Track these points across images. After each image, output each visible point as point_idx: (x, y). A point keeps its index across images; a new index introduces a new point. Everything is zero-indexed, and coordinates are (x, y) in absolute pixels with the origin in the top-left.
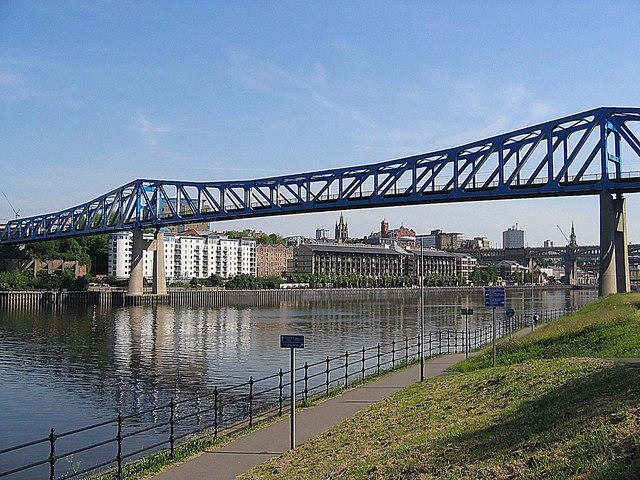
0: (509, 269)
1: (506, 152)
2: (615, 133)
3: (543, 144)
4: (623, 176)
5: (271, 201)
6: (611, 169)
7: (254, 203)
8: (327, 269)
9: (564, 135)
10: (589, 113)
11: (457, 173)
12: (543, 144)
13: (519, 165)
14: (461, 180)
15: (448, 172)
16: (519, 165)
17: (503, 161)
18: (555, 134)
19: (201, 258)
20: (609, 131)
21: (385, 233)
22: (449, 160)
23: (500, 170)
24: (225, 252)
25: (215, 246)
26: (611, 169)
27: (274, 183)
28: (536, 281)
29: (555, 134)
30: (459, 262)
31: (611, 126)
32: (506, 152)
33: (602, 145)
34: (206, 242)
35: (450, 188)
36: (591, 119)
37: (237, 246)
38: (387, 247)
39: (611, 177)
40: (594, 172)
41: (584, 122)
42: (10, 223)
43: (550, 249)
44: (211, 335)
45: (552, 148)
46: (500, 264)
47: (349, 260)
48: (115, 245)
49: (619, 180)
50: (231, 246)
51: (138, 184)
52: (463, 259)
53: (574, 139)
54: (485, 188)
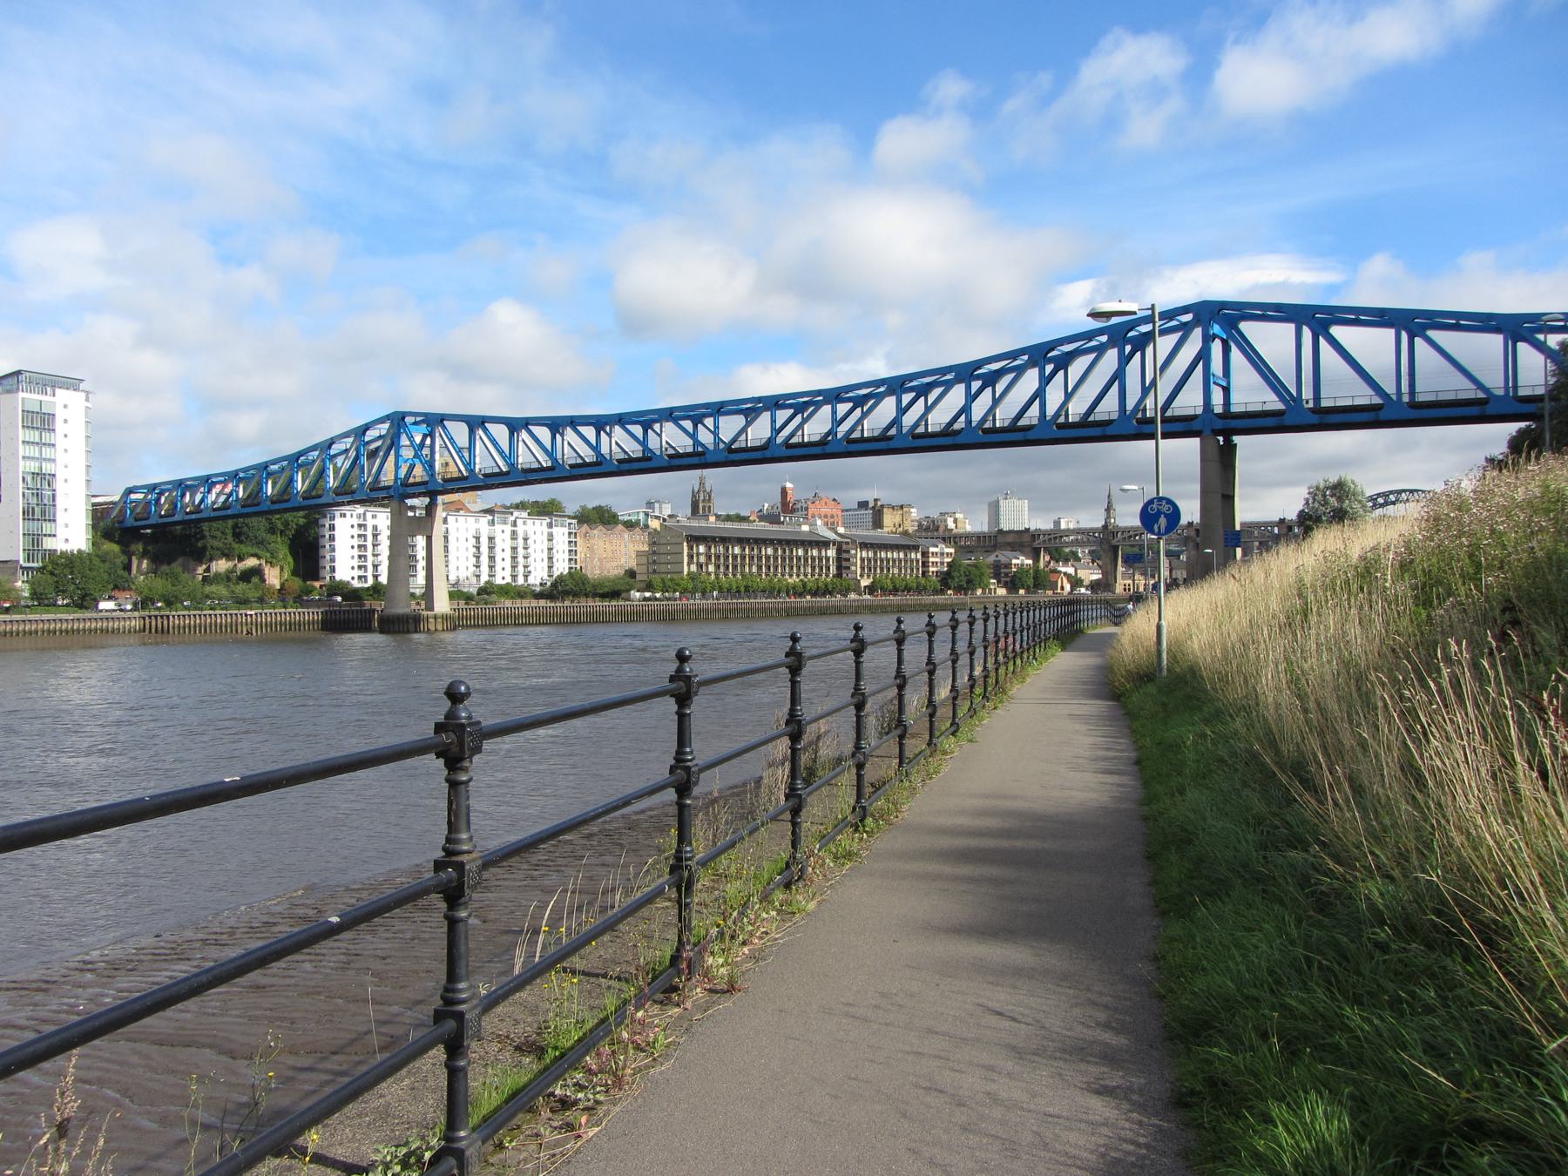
0: (1008, 566)
1: (976, 385)
2: (1223, 341)
3: (1112, 355)
4: (1234, 409)
5: (596, 449)
6: (1217, 398)
7: (569, 458)
8: (760, 568)
9: (1063, 363)
10: (1022, 351)
11: (902, 411)
12: (1112, 355)
13: (996, 402)
14: (977, 415)
15: (888, 408)
16: (996, 402)
17: (971, 398)
18: (1050, 361)
19: (484, 549)
20: (1215, 337)
21: (787, 506)
22: (958, 380)
23: (966, 410)
24: (526, 539)
25: (508, 528)
26: (1217, 398)
27: (647, 420)
28: (1054, 586)
29: (1131, 341)
30: (925, 554)
31: (1216, 329)
32: (976, 385)
33: (1203, 356)
34: (492, 523)
35: (957, 426)
36: (1188, 318)
37: (546, 530)
38: (805, 528)
39: (1218, 410)
40: (1190, 401)
41: (1174, 323)
42: (130, 491)
43: (505, 591)
44: (943, 703)
45: (1045, 380)
46: (992, 558)
47: (702, 549)
48: (332, 528)
49: (1227, 415)
50: (536, 528)
51: (398, 421)
52: (932, 550)
53: (1077, 368)
54: (1013, 427)
